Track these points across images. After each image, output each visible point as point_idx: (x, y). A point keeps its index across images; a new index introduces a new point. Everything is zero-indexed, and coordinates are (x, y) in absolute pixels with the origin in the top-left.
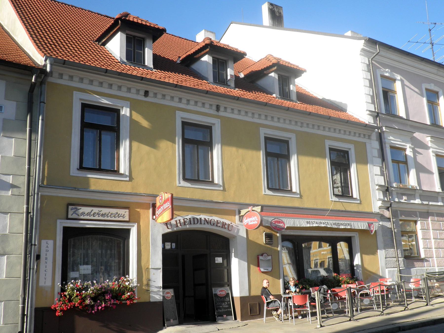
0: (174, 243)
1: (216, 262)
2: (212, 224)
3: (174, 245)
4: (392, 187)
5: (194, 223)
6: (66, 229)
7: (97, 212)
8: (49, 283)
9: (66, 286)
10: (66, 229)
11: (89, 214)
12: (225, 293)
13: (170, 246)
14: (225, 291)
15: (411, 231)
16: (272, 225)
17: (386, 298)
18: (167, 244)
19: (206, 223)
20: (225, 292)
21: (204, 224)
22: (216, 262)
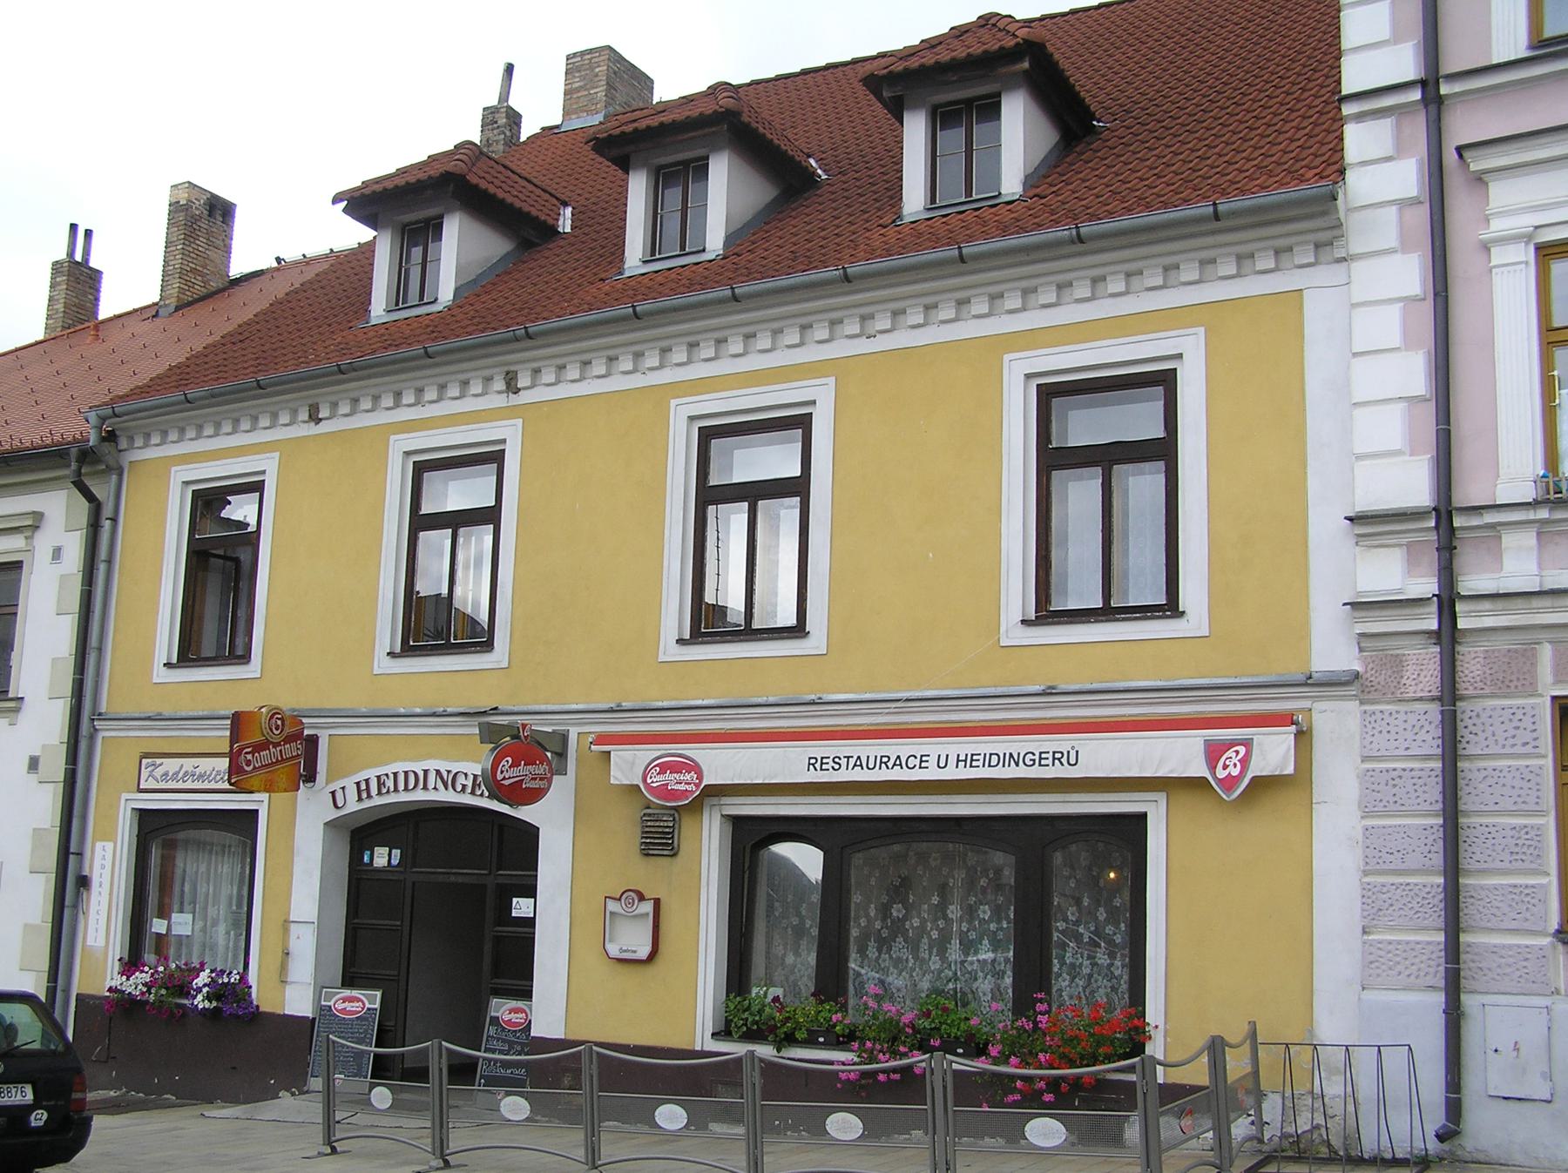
0: (397, 848)
1: (513, 915)
2: (459, 788)
3: (396, 853)
4: (1334, 1117)
5: (406, 789)
6: (144, 816)
7: (190, 769)
8: (101, 942)
9: (1128, 1050)
10: (144, 816)
11: (175, 777)
12: (363, 1009)
13: (387, 858)
14: (526, 1013)
15: (1457, 685)
16: (649, 781)
17: (473, 586)
18: (380, 852)
19: (440, 785)
20: (364, 1004)
21: (435, 788)
22: (513, 915)
